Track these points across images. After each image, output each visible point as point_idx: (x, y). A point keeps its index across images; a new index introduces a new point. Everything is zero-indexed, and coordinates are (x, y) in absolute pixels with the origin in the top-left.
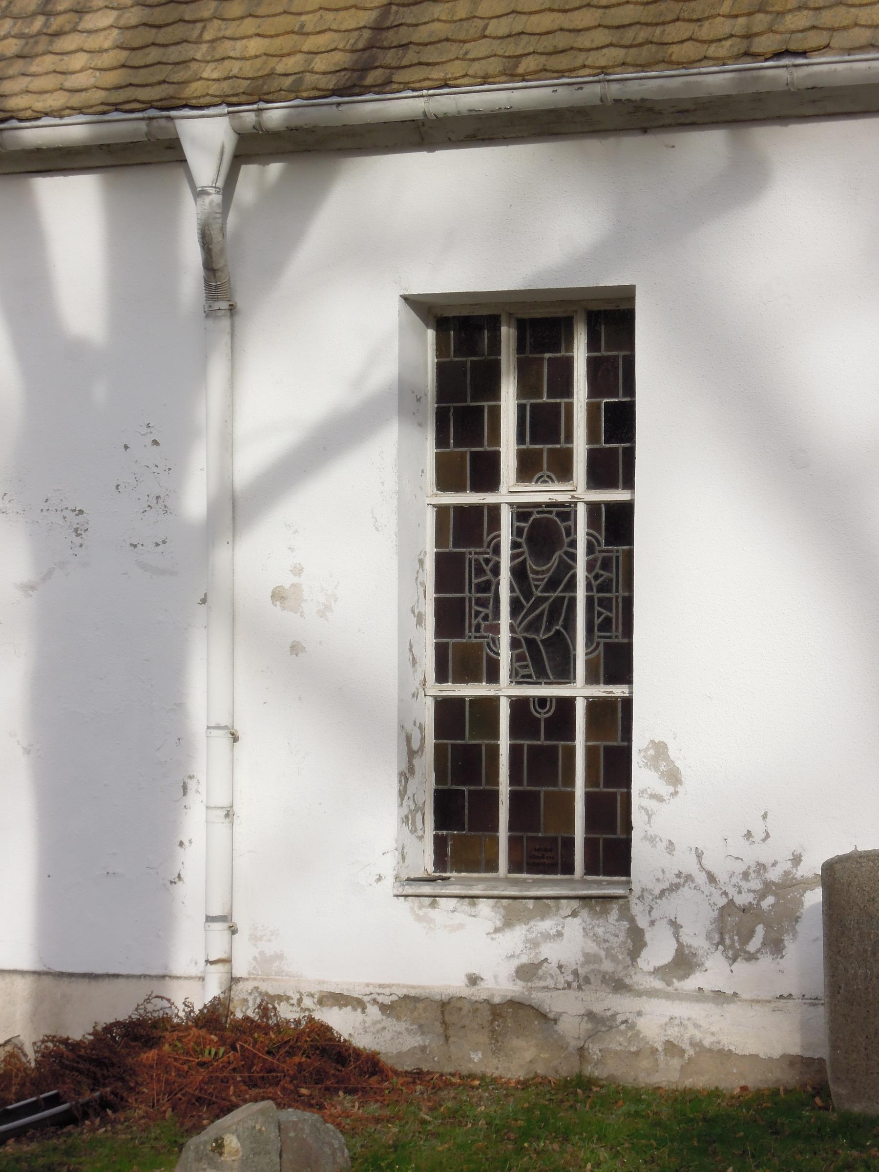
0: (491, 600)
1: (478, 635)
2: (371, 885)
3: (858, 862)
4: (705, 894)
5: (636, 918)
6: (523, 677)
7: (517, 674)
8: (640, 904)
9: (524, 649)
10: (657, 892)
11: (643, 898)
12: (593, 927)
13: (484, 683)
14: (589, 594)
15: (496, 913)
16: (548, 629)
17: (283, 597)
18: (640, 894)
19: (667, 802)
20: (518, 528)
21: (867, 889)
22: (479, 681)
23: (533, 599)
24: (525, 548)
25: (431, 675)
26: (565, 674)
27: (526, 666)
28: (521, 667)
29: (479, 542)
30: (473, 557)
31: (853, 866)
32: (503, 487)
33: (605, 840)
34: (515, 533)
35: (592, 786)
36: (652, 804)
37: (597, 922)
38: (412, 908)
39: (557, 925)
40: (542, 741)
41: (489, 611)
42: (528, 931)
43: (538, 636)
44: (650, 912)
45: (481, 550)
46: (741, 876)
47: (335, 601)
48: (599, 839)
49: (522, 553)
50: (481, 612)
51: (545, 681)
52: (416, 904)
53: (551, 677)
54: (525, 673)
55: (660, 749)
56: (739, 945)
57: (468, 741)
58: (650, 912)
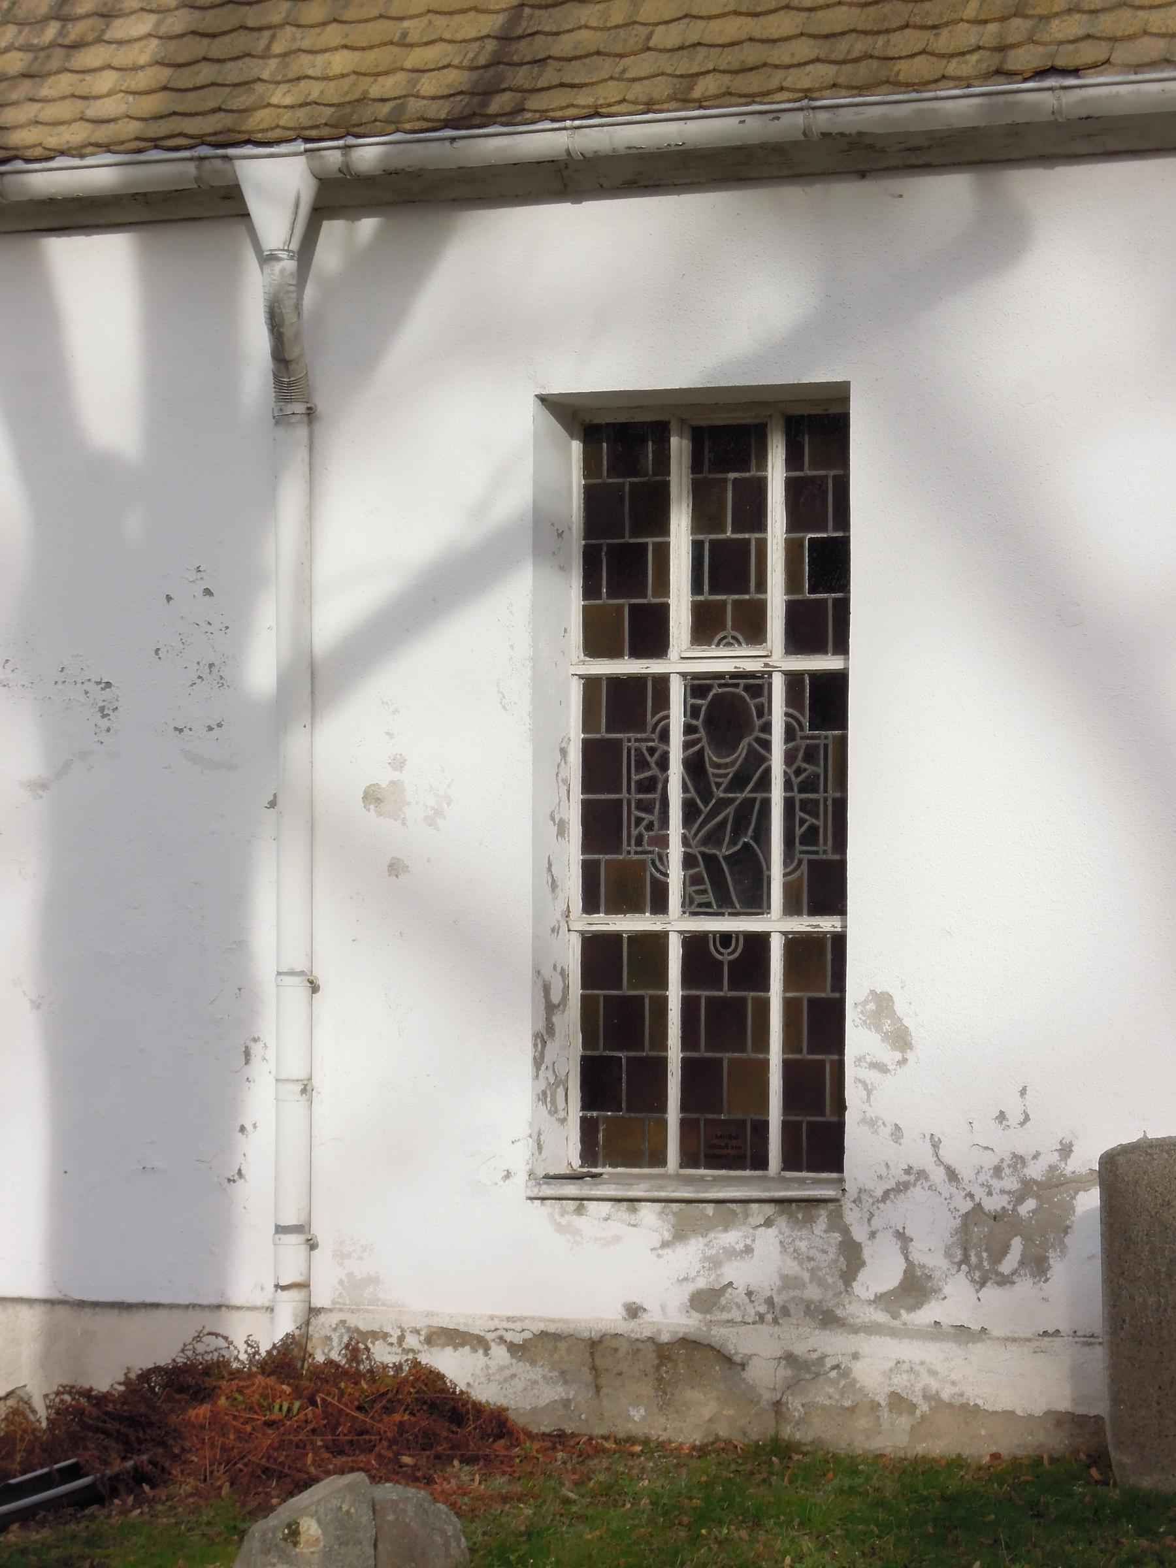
0: (658, 803)
1: (639, 849)
2: (496, 1184)
3: (1147, 1154)
4: (943, 1196)
5: (851, 1229)
6: (700, 905)
7: (691, 902)
8: (856, 1209)
9: (702, 868)
10: (879, 1193)
11: (860, 1202)
12: (793, 1240)
13: (647, 914)
14: (789, 794)
15: (664, 1221)
16: (733, 842)
17: (378, 799)
18: (856, 1196)
19: (893, 1073)
20: (693, 706)
21: (1160, 1189)
22: (641, 911)
23: (714, 801)
24: (702, 733)
25: (577, 903)
26: (756, 902)
27: (704, 892)
28: (697, 892)
29: (640, 725)
30: (633, 745)
31: (1142, 1158)
32: (674, 652)
33: (810, 1124)
34: (689, 714)
35: (792, 1052)
36: (873, 1076)
37: (799, 1234)
38: (551, 1215)
39: (745, 1237)
40: (725, 992)
41: (654, 818)
42: (706, 1245)
43: (720, 850)
44: (869, 1220)
45: (644, 736)
46: (992, 1171)
47: (449, 804)
48: (801, 1122)
49: (699, 740)
50: (643, 819)
51: (729, 910)
52: (557, 1210)
53: (738, 906)
54: (702, 901)
55: (883, 1003)
56: (989, 1264)
57: (626, 991)
58: (869, 1220)
